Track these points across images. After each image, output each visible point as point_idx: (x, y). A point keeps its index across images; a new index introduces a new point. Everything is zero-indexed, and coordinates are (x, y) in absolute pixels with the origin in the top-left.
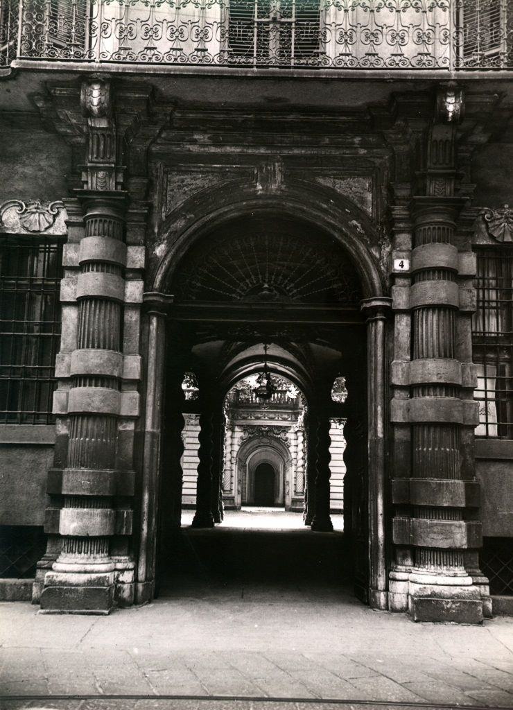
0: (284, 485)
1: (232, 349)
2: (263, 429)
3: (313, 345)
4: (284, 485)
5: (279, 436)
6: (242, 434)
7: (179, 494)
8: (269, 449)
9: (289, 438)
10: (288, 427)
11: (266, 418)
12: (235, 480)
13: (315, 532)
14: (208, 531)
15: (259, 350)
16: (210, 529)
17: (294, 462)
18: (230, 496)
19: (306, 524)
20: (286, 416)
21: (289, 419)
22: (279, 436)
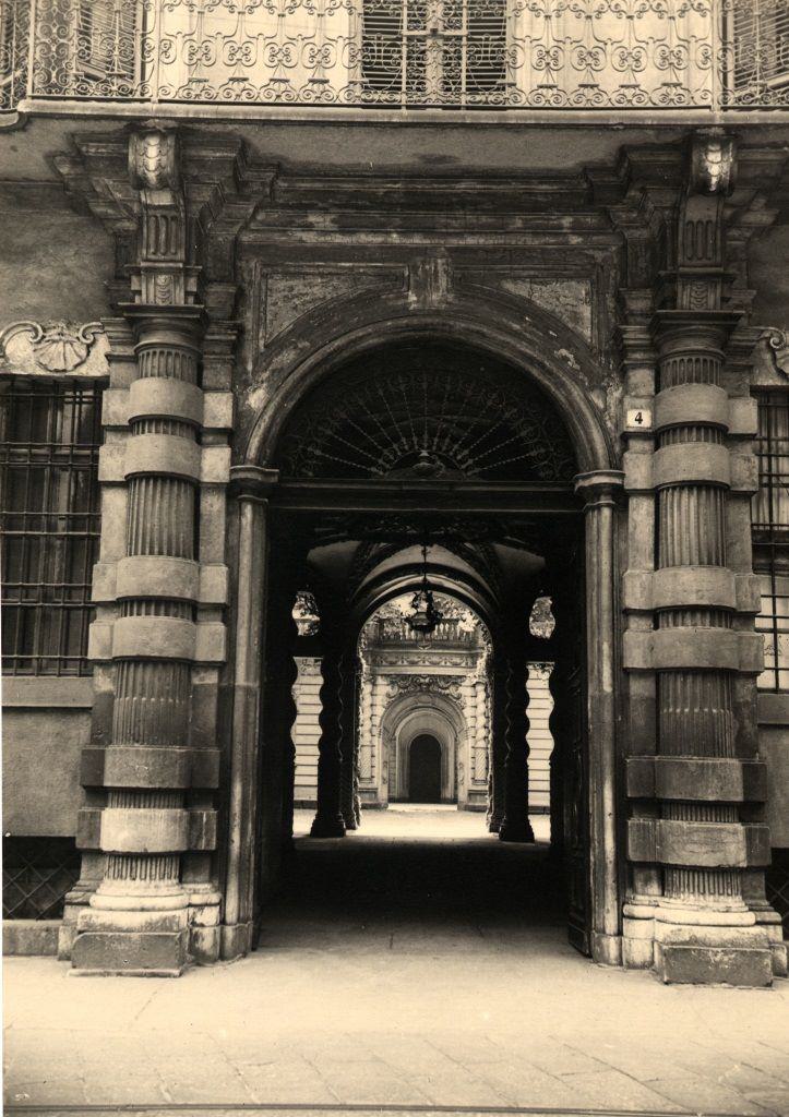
3: (500, 548)
5: (447, 692)
6: (389, 689)
9: (463, 693)
12: (378, 762)
15: (413, 555)
21: (463, 665)
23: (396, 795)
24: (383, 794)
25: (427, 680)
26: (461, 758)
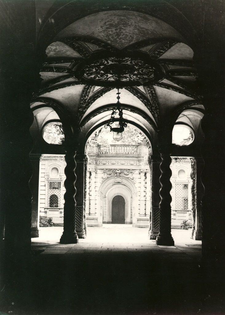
1: (90, 96)
3: (159, 90)
5: (128, 176)
6: (103, 175)
7: (200, 174)
9: (135, 177)
12: (98, 206)
13: (160, 246)
15: (110, 97)
17: (139, 194)
21: (135, 165)
23: (106, 220)
24: (100, 221)
25: (119, 171)
26: (134, 205)
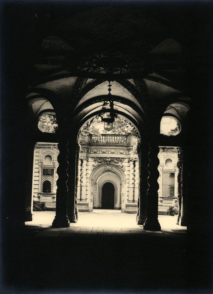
0: (120, 196)
1: (82, 87)
2: (107, 160)
4: (120, 196)
5: (118, 164)
6: (94, 163)
8: (110, 173)
10: (123, 158)
11: (109, 153)
12: (89, 193)
14: (62, 232)
15: (102, 89)
16: (65, 229)
17: (128, 181)
18: (85, 203)
19: (139, 224)
20: (122, 151)
21: (125, 153)
22: (118, 164)
